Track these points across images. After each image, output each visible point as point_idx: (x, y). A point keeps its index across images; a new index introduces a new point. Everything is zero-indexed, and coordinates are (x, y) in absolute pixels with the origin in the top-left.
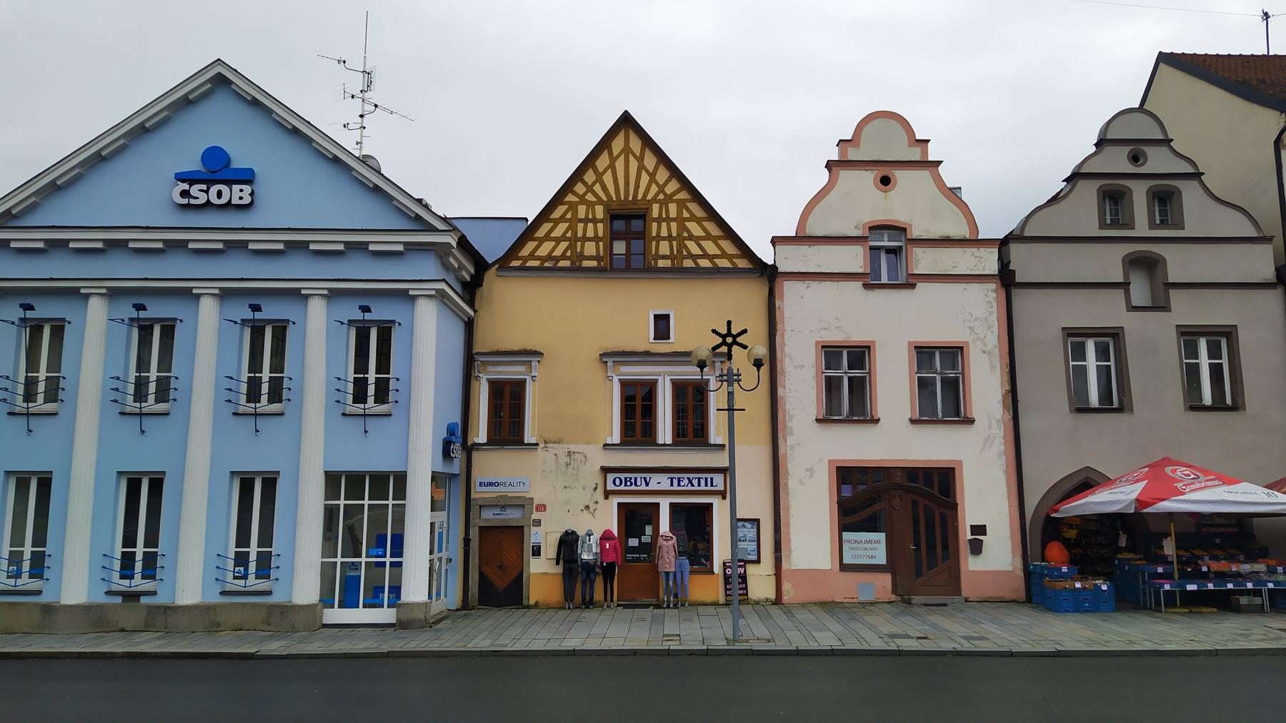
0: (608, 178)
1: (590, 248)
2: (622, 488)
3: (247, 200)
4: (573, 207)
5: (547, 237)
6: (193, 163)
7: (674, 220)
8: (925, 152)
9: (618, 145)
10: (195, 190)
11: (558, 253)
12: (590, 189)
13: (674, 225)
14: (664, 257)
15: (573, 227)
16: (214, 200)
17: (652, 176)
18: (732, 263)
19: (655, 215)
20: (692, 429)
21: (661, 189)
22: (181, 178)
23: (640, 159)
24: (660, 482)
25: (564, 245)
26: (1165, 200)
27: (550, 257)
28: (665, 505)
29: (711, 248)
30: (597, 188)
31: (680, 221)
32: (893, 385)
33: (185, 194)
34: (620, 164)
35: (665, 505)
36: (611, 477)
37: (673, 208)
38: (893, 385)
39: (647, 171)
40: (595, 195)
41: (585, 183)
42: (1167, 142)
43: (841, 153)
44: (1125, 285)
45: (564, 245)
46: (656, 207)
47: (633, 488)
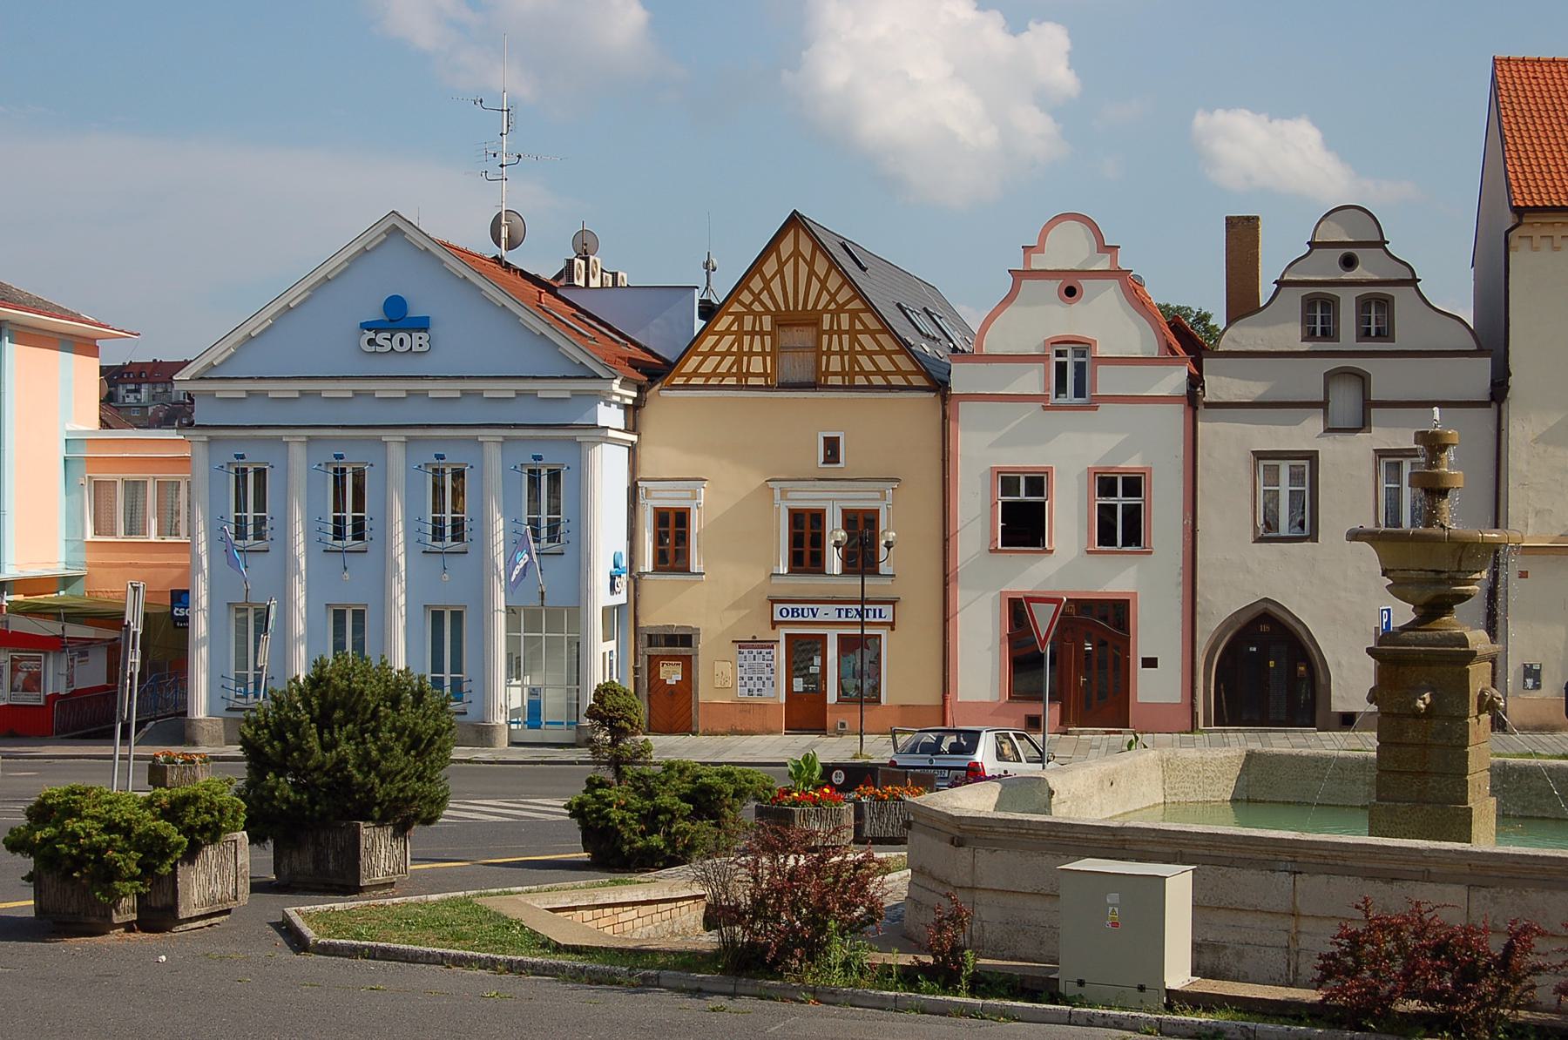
0: (776, 285)
1: (757, 365)
2: (789, 618)
3: (426, 347)
4: (739, 317)
5: (712, 352)
6: (375, 314)
7: (846, 332)
8: (1114, 260)
9: (786, 247)
10: (380, 338)
11: (723, 369)
12: (757, 297)
13: (845, 338)
14: (835, 374)
15: (739, 362)
16: (397, 347)
17: (823, 283)
18: (907, 380)
19: (826, 327)
20: (862, 557)
21: (833, 298)
22: (367, 326)
23: (811, 264)
24: (828, 612)
25: (729, 360)
26: (1376, 312)
27: (714, 374)
28: (833, 636)
29: (884, 363)
30: (765, 297)
31: (853, 333)
32: (1069, 516)
33: (371, 342)
34: (788, 270)
35: (833, 636)
36: (777, 607)
37: (845, 318)
38: (1069, 516)
39: (818, 277)
40: (762, 304)
41: (752, 292)
42: (1381, 244)
43: (1027, 261)
44: (1324, 405)
45: (729, 360)
46: (826, 317)
47: (801, 619)
